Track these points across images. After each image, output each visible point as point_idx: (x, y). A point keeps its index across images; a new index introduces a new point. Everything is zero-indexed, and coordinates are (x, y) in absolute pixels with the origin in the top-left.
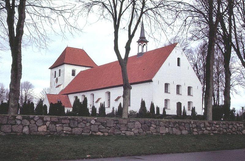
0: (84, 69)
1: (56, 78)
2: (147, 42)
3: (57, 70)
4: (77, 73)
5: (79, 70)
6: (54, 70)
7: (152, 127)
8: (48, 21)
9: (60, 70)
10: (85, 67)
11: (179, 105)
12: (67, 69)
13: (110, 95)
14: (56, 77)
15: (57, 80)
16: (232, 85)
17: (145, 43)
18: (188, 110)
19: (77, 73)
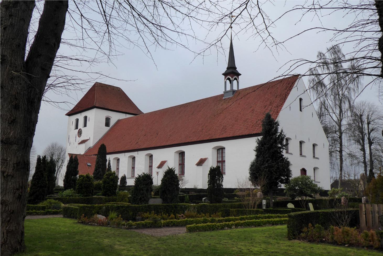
0: (122, 116)
1: (77, 130)
2: (239, 75)
3: (80, 117)
4: (112, 123)
5: (115, 117)
6: (74, 118)
7: (346, 61)
8: (95, 63)
9: (86, 118)
10: (125, 114)
11: (304, 171)
12: (96, 117)
13: (119, 162)
14: (79, 129)
15: (80, 133)
16: (59, 159)
17: (236, 77)
18: (286, 152)
19: (112, 123)
